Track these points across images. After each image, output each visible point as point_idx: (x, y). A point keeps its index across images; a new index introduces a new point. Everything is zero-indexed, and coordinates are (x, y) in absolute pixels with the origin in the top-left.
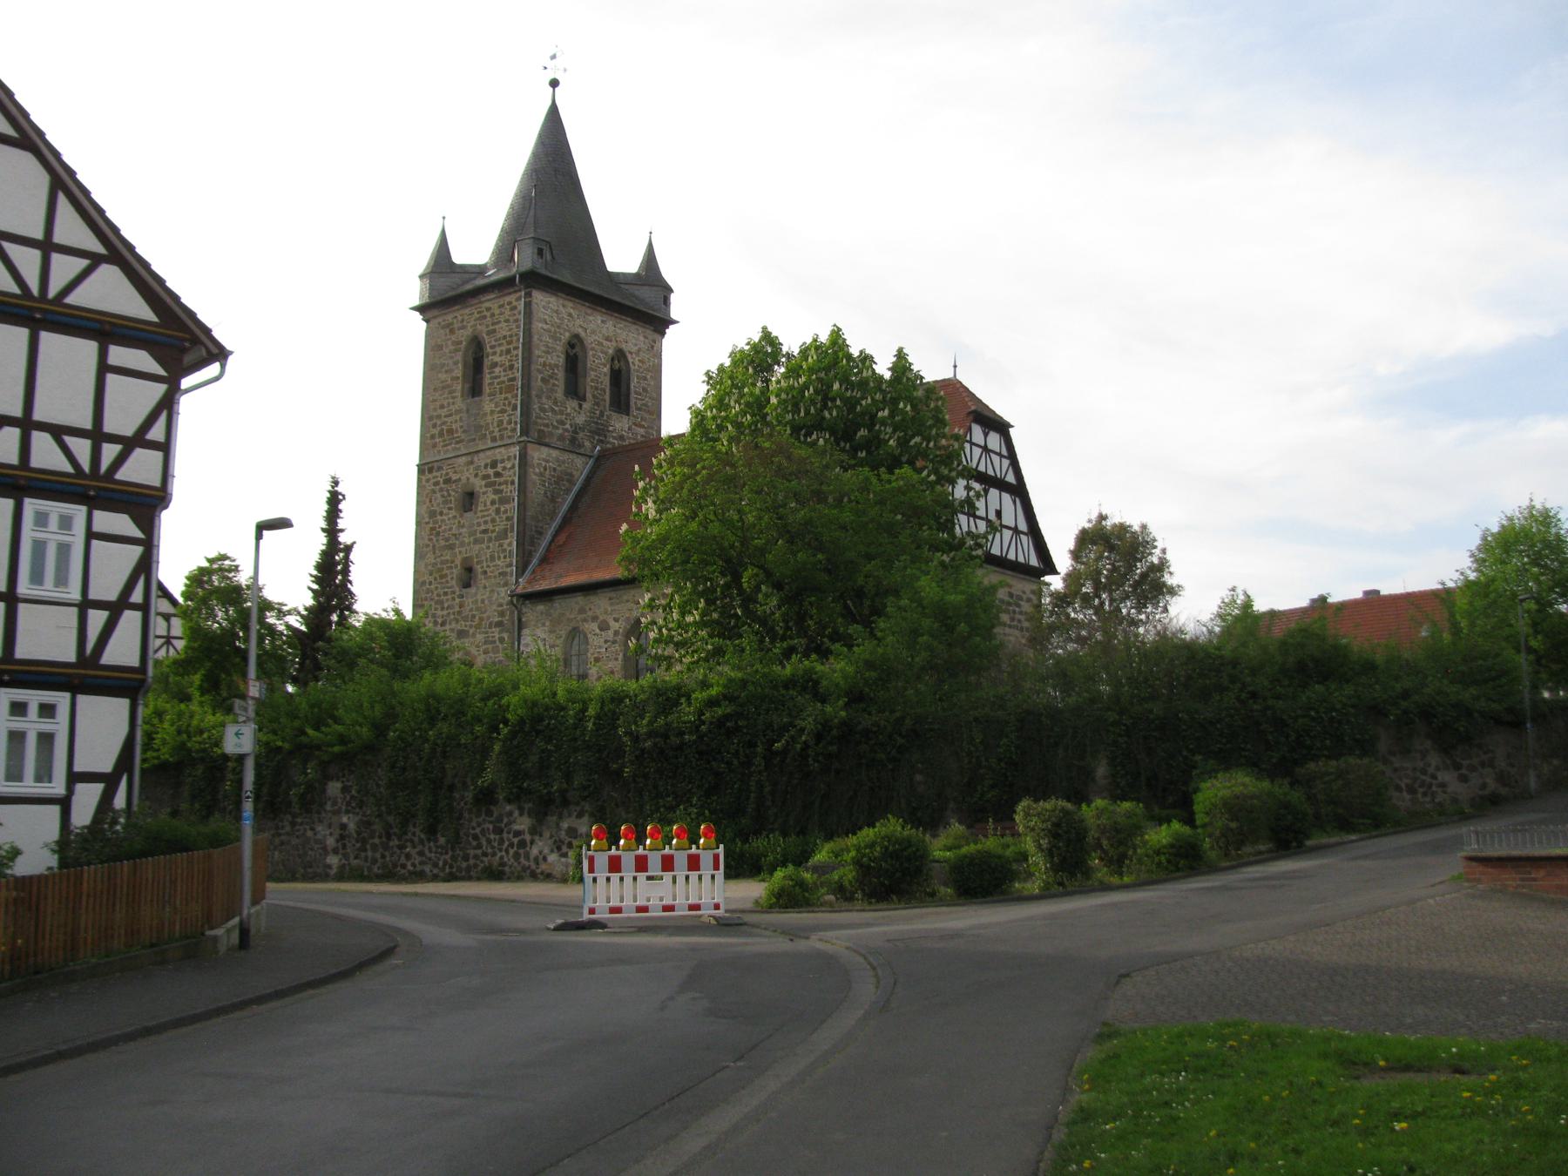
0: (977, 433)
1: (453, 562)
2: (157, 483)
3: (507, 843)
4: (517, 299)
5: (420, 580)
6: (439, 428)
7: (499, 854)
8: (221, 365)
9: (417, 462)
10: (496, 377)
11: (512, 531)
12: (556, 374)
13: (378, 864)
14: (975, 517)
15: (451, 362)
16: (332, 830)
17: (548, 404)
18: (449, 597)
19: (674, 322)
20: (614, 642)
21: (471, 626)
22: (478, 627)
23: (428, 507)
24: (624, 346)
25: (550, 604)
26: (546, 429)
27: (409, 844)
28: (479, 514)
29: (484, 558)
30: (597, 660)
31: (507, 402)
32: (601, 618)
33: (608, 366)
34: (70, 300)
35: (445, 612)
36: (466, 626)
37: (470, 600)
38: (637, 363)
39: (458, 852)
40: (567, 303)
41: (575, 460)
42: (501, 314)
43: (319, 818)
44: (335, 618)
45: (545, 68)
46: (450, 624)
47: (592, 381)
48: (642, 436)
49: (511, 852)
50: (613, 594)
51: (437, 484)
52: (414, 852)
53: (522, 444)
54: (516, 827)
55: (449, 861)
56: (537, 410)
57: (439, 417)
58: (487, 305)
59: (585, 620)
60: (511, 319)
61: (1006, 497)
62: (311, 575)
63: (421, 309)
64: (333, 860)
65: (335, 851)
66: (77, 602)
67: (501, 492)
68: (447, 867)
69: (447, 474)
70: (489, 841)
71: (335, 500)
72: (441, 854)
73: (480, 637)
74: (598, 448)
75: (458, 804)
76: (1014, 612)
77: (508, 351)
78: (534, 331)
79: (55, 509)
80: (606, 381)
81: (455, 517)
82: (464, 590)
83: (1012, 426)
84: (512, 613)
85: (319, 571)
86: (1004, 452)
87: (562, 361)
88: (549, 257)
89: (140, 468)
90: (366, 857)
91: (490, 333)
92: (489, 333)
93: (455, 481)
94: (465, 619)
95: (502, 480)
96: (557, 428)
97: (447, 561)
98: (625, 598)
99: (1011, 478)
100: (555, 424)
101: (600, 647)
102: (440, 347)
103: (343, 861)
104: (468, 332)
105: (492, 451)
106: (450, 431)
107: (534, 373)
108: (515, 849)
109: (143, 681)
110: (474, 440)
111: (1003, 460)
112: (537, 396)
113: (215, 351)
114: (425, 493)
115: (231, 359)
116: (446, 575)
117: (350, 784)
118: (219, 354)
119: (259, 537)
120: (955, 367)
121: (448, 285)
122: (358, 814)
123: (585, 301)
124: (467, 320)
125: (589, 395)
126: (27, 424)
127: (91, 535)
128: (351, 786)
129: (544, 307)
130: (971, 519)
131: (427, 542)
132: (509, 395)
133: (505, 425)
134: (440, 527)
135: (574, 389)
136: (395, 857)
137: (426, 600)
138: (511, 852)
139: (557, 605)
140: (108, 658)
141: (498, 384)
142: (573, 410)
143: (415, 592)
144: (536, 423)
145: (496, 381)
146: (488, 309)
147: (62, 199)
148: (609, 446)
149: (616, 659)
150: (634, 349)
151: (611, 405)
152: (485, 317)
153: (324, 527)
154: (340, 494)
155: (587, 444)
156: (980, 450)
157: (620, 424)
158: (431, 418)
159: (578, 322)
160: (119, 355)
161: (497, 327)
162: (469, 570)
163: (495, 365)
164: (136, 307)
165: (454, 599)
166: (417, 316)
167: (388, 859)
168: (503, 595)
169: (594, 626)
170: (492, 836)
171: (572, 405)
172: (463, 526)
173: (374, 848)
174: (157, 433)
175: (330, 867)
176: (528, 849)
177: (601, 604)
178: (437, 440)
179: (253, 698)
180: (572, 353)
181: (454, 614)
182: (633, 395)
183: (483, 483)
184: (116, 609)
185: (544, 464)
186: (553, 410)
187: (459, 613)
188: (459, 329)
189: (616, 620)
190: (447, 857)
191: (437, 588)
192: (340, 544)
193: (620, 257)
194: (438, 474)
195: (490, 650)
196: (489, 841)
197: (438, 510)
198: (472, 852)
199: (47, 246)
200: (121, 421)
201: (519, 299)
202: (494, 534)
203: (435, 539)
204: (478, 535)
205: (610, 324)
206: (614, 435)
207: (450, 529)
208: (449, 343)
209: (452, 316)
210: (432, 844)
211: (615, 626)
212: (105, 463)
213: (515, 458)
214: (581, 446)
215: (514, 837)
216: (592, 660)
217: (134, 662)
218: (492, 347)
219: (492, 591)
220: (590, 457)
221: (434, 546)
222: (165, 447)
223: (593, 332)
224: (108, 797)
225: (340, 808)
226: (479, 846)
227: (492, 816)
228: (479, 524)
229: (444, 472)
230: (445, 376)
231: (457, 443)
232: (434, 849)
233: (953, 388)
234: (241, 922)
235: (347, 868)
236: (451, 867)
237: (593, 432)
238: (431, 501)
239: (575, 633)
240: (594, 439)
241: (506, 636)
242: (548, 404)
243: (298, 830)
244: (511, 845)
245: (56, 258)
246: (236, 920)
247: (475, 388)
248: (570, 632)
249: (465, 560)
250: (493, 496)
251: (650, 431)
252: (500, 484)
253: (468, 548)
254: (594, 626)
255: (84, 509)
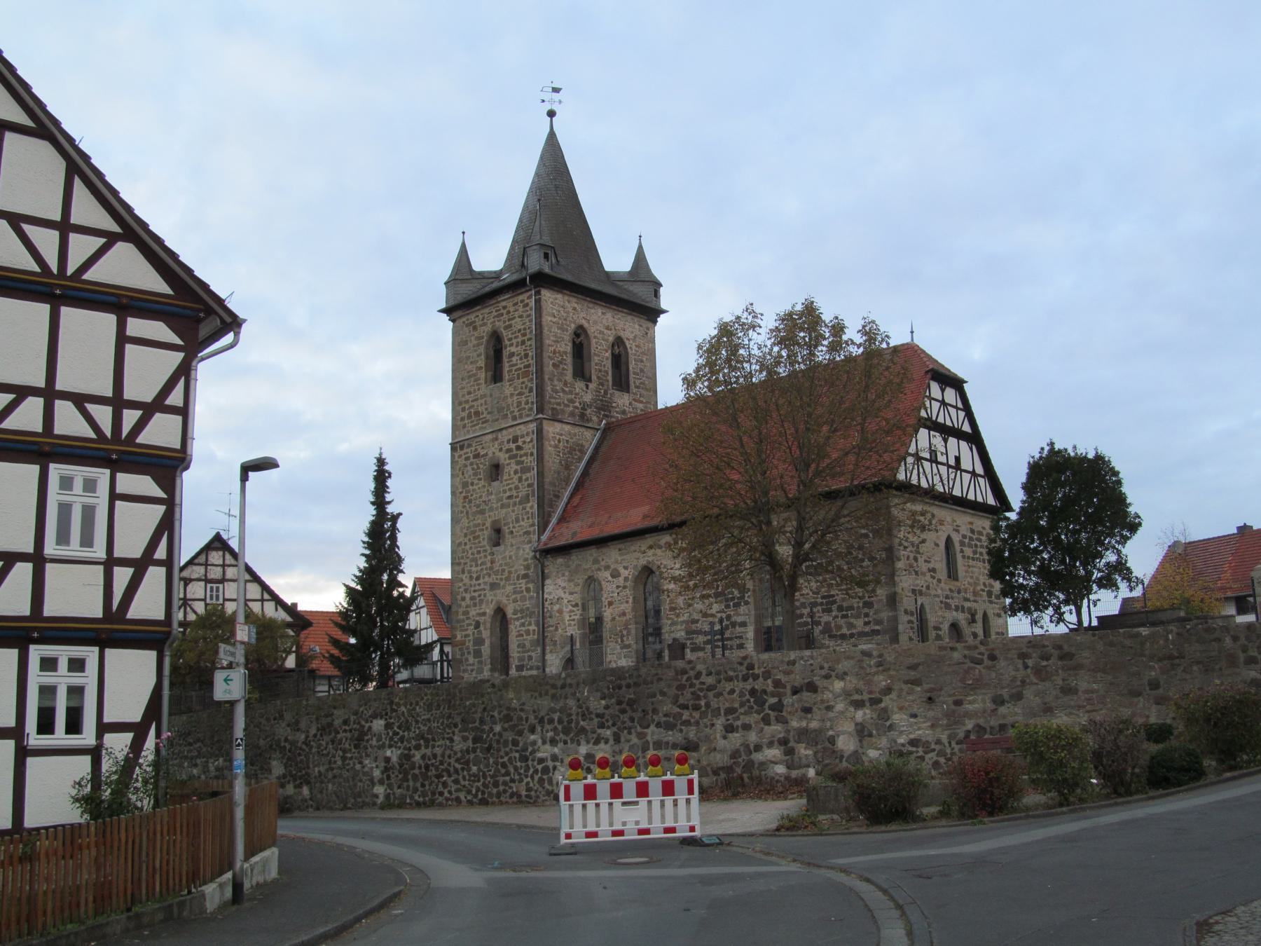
0: (935, 389)
1: (484, 524)
2: (177, 445)
3: (531, 771)
4: (528, 298)
5: (457, 542)
6: (467, 412)
7: (525, 781)
8: (235, 335)
9: (450, 441)
10: (513, 365)
11: (533, 496)
12: (565, 360)
13: (419, 793)
14: (938, 463)
15: (475, 354)
16: (377, 763)
17: (559, 386)
18: (482, 555)
19: (664, 312)
20: (625, 587)
21: (501, 579)
22: (508, 579)
23: (461, 479)
24: (622, 334)
25: (567, 557)
26: (558, 407)
27: (445, 774)
28: (505, 483)
29: (510, 520)
30: (610, 604)
31: (524, 386)
32: (612, 567)
33: (610, 351)
34: (88, 276)
35: (479, 568)
36: (497, 579)
37: (500, 557)
38: (634, 347)
39: (489, 779)
40: (571, 299)
41: (585, 433)
42: (516, 310)
43: (366, 753)
44: (385, 577)
45: (543, 101)
46: (484, 578)
47: (596, 364)
48: (642, 410)
49: (536, 778)
50: (622, 546)
51: (467, 459)
52: (449, 781)
53: (539, 421)
54: (540, 755)
55: (481, 788)
56: (550, 391)
57: (467, 402)
58: (504, 304)
59: (599, 569)
60: (525, 315)
61: (963, 444)
62: (364, 542)
63: (446, 311)
64: (380, 790)
65: (381, 782)
66: (103, 560)
67: (522, 462)
68: (480, 793)
69: (476, 450)
70: (516, 769)
71: (382, 477)
72: (474, 781)
73: (509, 589)
74: (604, 422)
75: (488, 736)
76: (976, 546)
77: (523, 343)
78: (544, 323)
79: (80, 473)
80: (608, 364)
81: (484, 486)
82: (495, 549)
83: (966, 382)
84: (536, 566)
85: (370, 538)
86: (960, 405)
87: (569, 348)
88: (554, 261)
89: (162, 432)
90: (408, 787)
91: (507, 328)
92: (507, 328)
93: (483, 456)
94: (496, 573)
95: (522, 452)
96: (568, 406)
97: (479, 524)
98: (633, 548)
99: (967, 428)
100: (566, 402)
101: (613, 592)
102: (465, 343)
103: (388, 791)
104: (488, 328)
105: (514, 429)
106: (477, 413)
107: (546, 360)
108: (540, 775)
109: (169, 633)
110: (497, 420)
111: (959, 412)
112: (549, 379)
113: (229, 320)
114: (458, 468)
115: (244, 327)
116: (479, 536)
117: (392, 721)
118: (232, 323)
119: (244, 478)
120: (912, 332)
121: (468, 290)
122: (400, 748)
123: (587, 296)
124: (487, 319)
125: (594, 377)
126: (50, 393)
127: (114, 496)
128: (393, 723)
129: (552, 303)
130: (934, 465)
131: (461, 508)
132: (525, 380)
133: (523, 406)
134: (472, 495)
135: (581, 372)
136: (434, 786)
137: (462, 558)
138: (536, 778)
139: (573, 557)
140: (134, 612)
141: (516, 371)
142: (586, 394)
143: (453, 552)
144: (550, 402)
145: (514, 368)
146: (504, 308)
147: (78, 183)
148: (613, 420)
149: (627, 602)
150: (631, 336)
151: (613, 385)
152: (502, 315)
153: (373, 500)
154: (387, 471)
155: (594, 418)
156: (939, 404)
157: (622, 401)
158: (460, 404)
159: (582, 315)
160: (136, 326)
161: (513, 322)
162: (498, 531)
163: (512, 355)
164: (151, 281)
165: (486, 556)
166: (445, 317)
167: (427, 787)
168: (527, 551)
169: (607, 574)
170: (518, 764)
171: (580, 385)
172: (492, 494)
173: (415, 777)
174: (175, 398)
175: (377, 796)
176: (551, 774)
177: (612, 555)
178: (466, 421)
179: (242, 643)
180: (578, 341)
181: (486, 569)
182: (632, 376)
183: (507, 456)
184: (140, 566)
185: (558, 437)
186: (564, 391)
187: (491, 568)
188: (481, 326)
189: (626, 568)
190: (479, 784)
191: (471, 548)
192: (388, 514)
193: (615, 260)
194: (469, 450)
195: (518, 599)
196: (516, 769)
197: (470, 481)
198: (501, 779)
199: (65, 227)
200: (141, 386)
201: (530, 297)
202: (518, 500)
203: (468, 506)
204: (505, 501)
205: (609, 315)
206: (617, 410)
207: (481, 497)
208: (473, 338)
209: (474, 315)
210: (465, 773)
211: (624, 573)
212: (126, 429)
213: (533, 434)
214: (589, 420)
215: (538, 764)
216: (606, 603)
217: (160, 615)
218: (510, 340)
219: (518, 548)
220: (598, 430)
221: (467, 513)
222: (184, 412)
223: (595, 322)
224: (137, 746)
225: (384, 743)
226: (507, 774)
227: (518, 746)
228: (505, 491)
229: (473, 449)
230: (470, 366)
231: (483, 423)
232: (467, 777)
233: (910, 352)
234: (234, 876)
235: (392, 797)
236: (483, 793)
237: (599, 409)
238: (463, 474)
239: (591, 581)
240: (600, 413)
241: (531, 586)
242: (559, 386)
243: (349, 764)
244: (536, 771)
245: (73, 238)
246: (229, 875)
247: (496, 376)
248: (586, 580)
249: (494, 522)
250: (516, 467)
251: (649, 406)
252: (521, 456)
253: (497, 512)
254: (607, 574)
255: (108, 472)
